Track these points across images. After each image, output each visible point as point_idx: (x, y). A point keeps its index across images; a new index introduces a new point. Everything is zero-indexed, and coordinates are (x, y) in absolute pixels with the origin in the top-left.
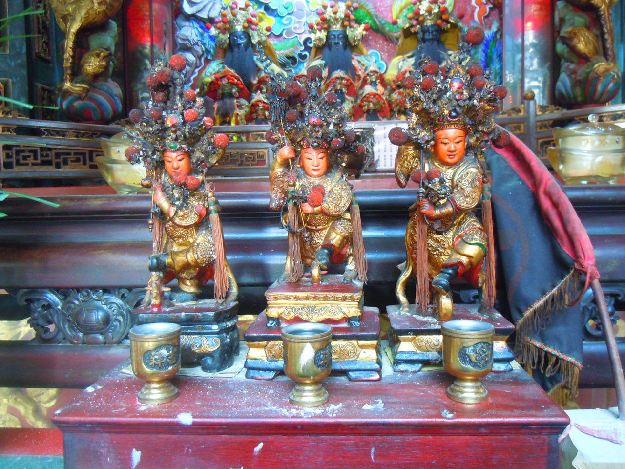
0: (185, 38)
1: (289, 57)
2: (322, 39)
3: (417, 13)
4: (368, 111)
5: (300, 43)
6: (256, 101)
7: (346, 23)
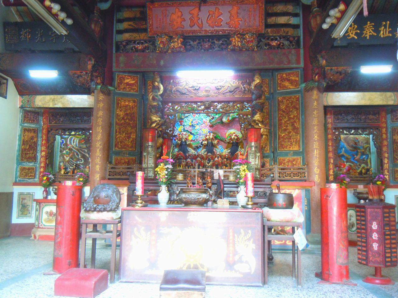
1: (196, 147)
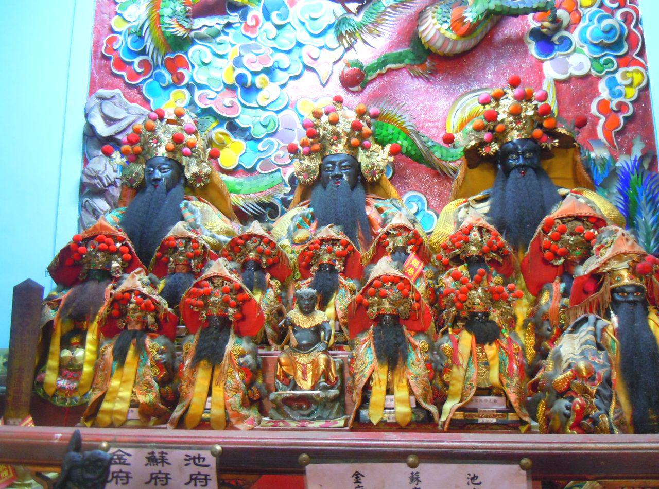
0: (94, 174)
1: (262, 205)
3: (492, 117)
4: (379, 319)
5: (284, 180)
6: (123, 292)
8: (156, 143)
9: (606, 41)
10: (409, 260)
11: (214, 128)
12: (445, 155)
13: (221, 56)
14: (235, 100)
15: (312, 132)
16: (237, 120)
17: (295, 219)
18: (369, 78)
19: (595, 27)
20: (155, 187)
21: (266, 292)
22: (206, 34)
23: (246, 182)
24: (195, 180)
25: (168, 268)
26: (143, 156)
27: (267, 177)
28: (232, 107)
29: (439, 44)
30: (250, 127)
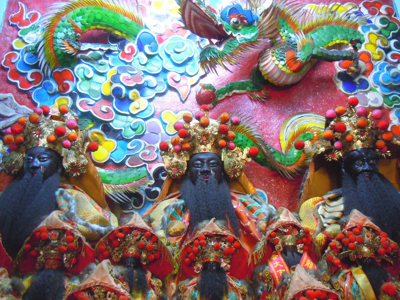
1: (129, 194)
2: (182, 167)
5: (149, 174)
7: (222, 142)
8: (39, 134)
9: (393, 84)
10: (304, 261)
11: (91, 129)
12: (283, 160)
13: (101, 74)
14: (110, 108)
15: (183, 133)
16: (111, 124)
17: (168, 210)
18: (219, 99)
19: (385, 74)
20: (33, 174)
21: (147, 294)
22: (90, 57)
23: (116, 174)
24: (72, 170)
25: (36, 262)
26: (24, 145)
27: (135, 171)
28: (107, 112)
29: (276, 76)
30: (121, 130)
